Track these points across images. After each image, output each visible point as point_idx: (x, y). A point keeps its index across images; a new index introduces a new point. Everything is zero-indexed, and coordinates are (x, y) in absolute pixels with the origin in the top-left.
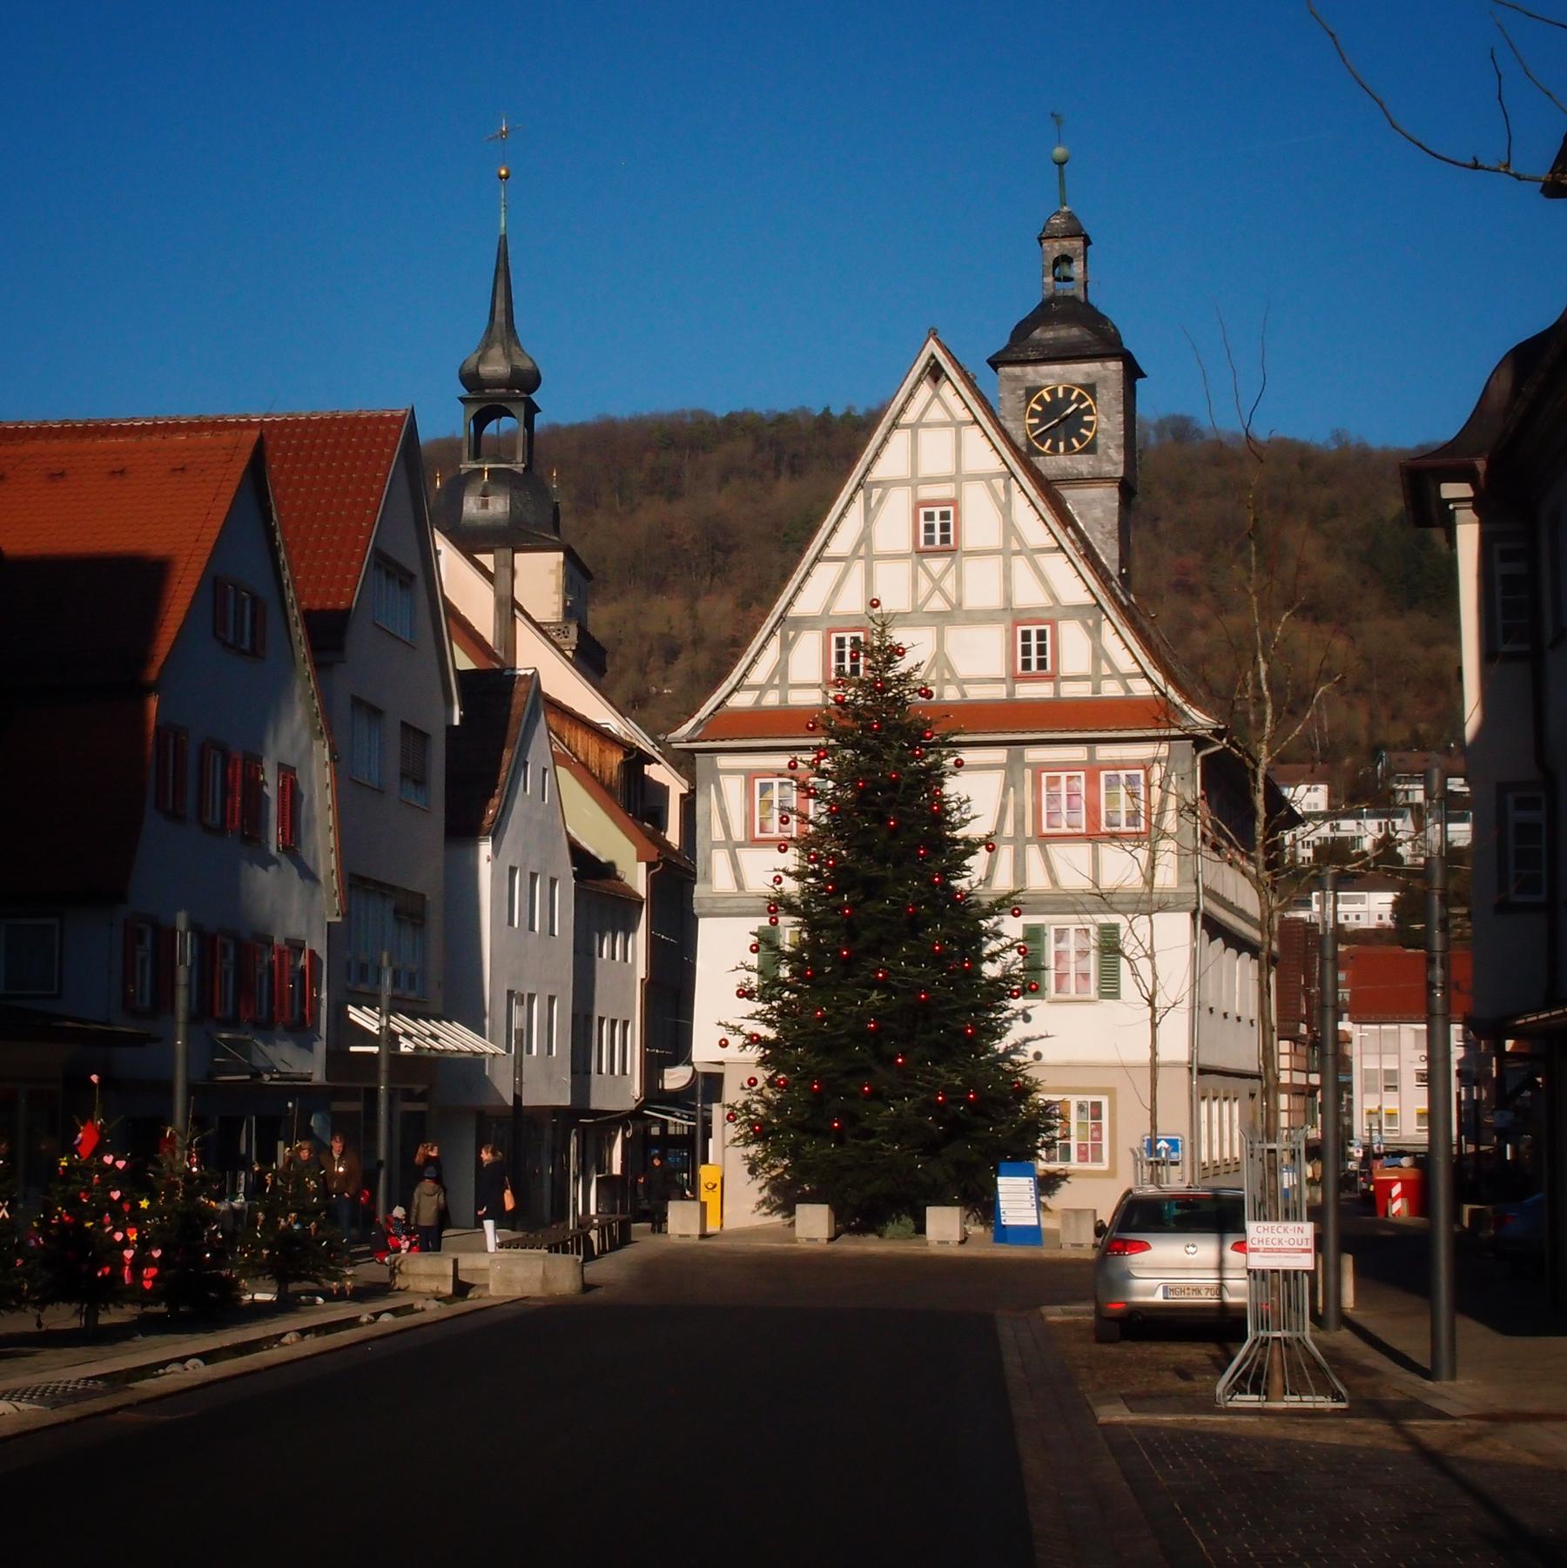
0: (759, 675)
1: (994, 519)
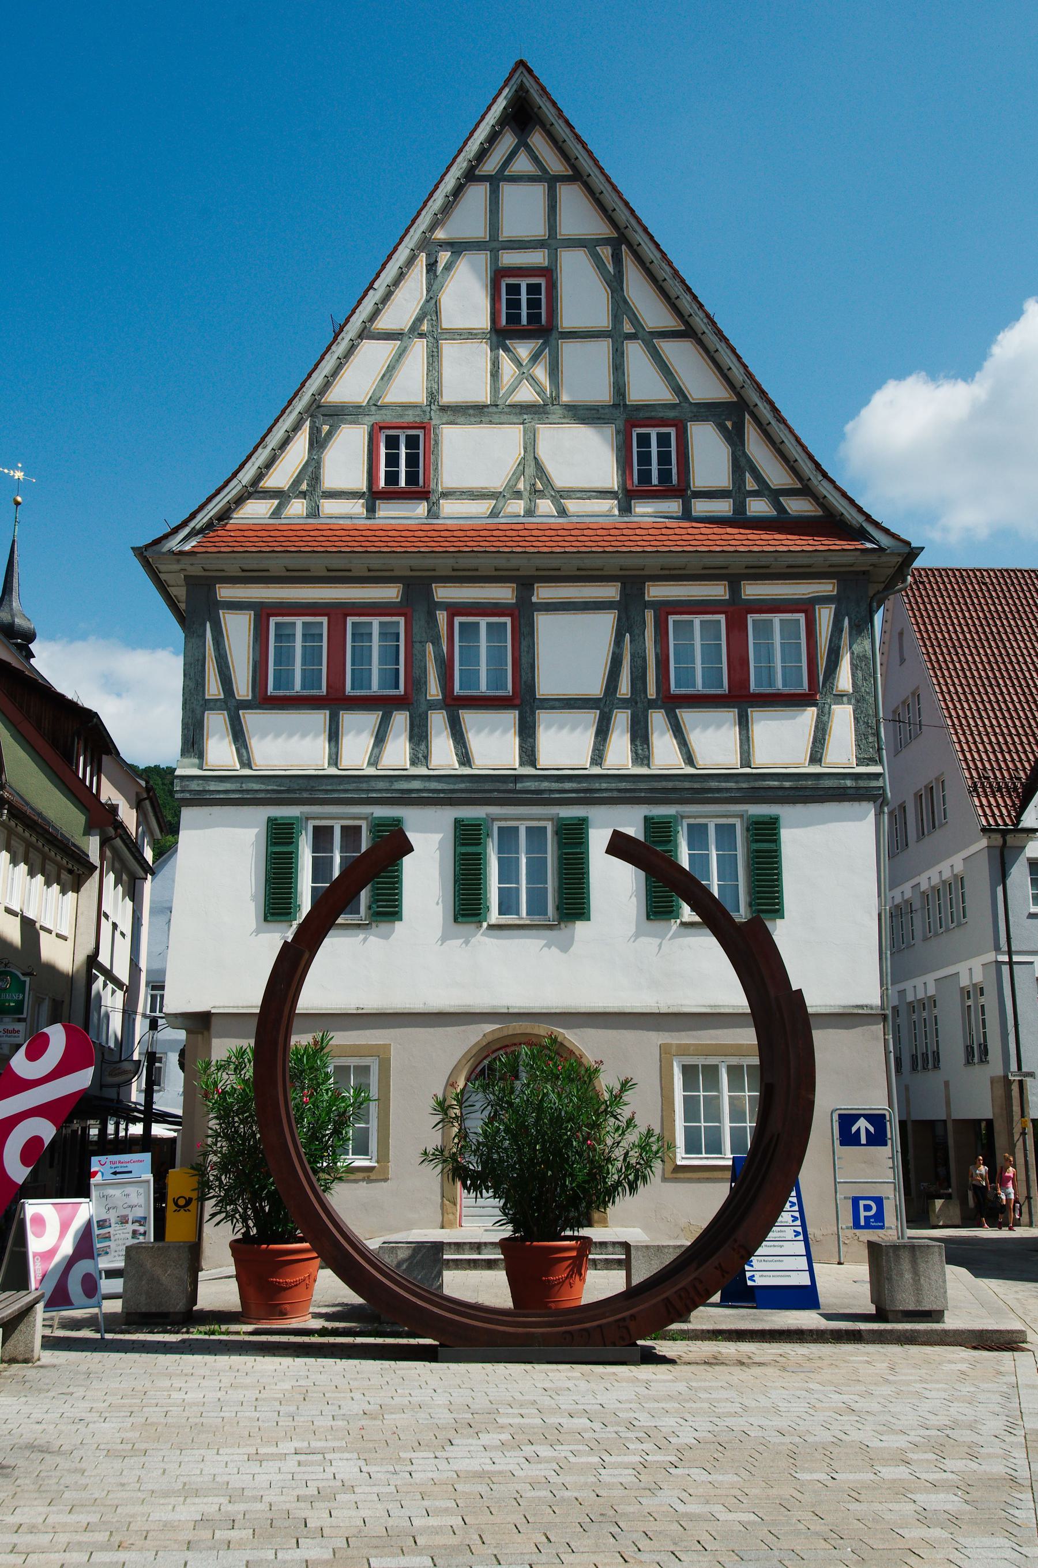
0: (280, 478)
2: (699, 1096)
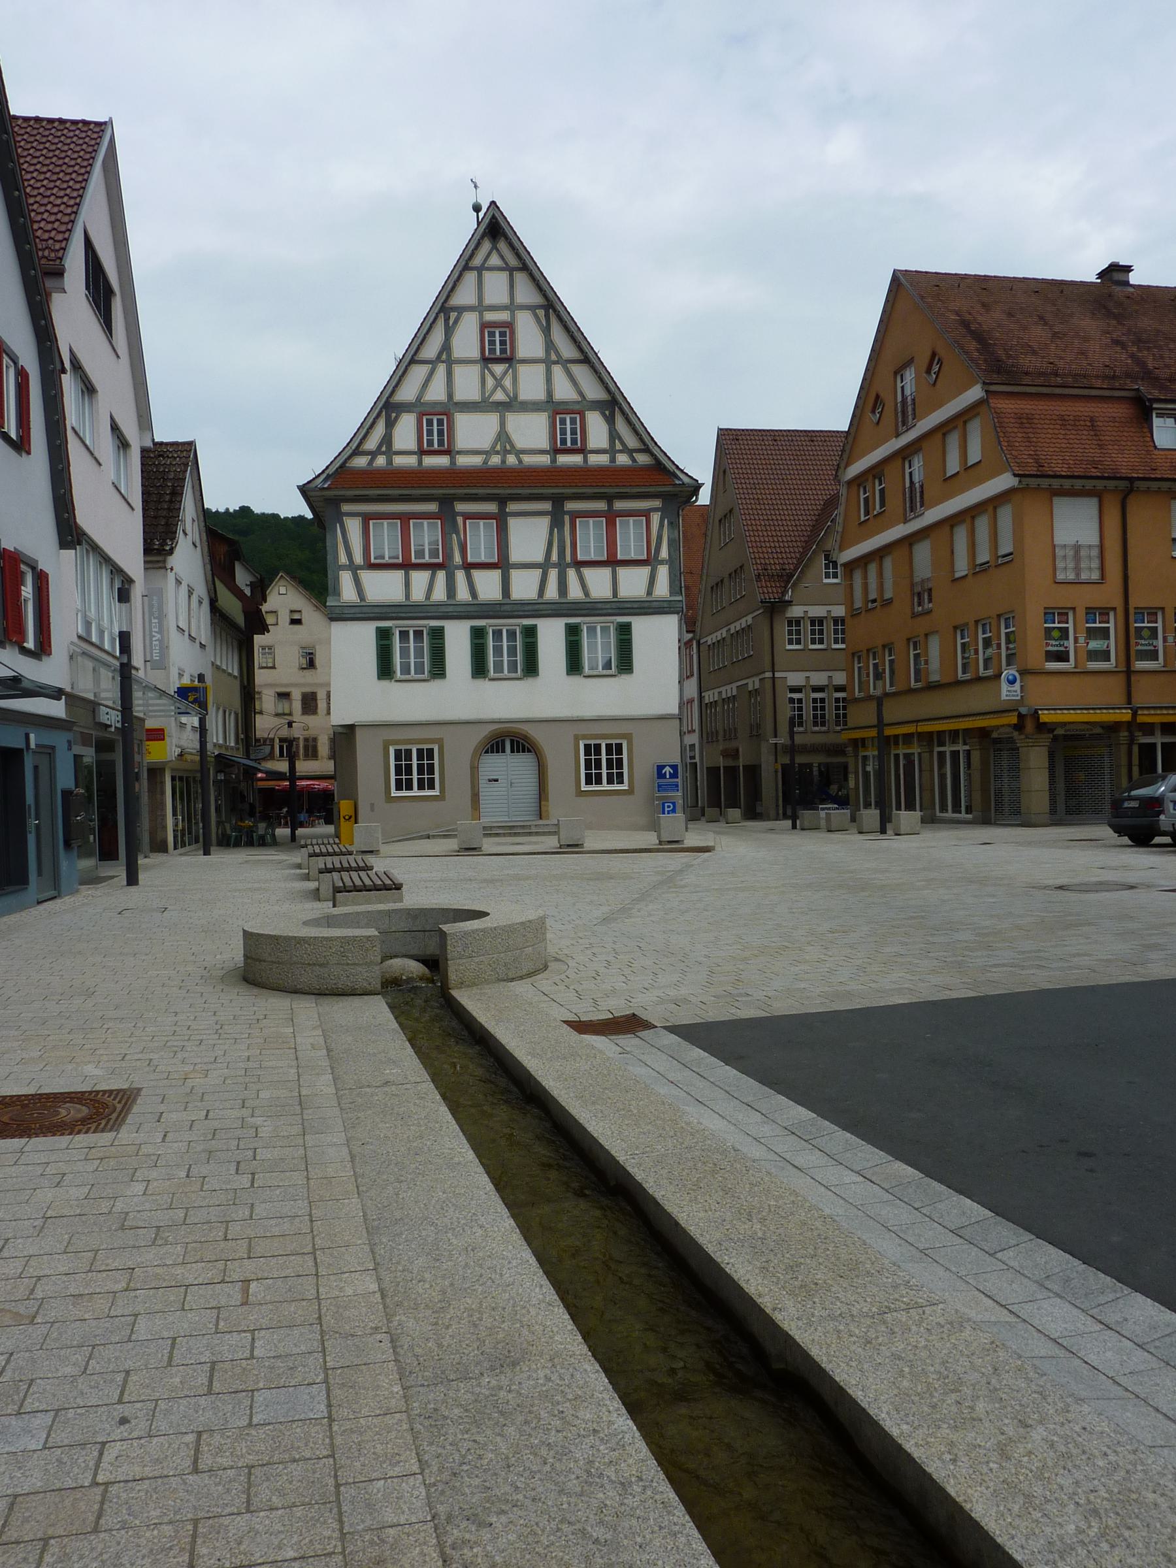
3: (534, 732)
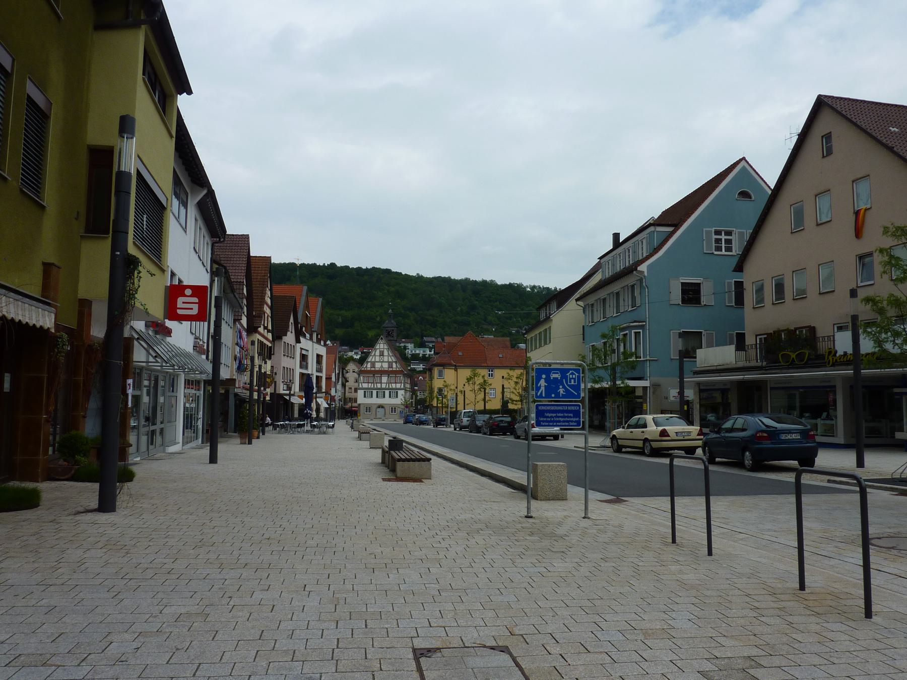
0: (364, 367)
1: (387, 353)
2: (721, 239)
3: (385, 406)
